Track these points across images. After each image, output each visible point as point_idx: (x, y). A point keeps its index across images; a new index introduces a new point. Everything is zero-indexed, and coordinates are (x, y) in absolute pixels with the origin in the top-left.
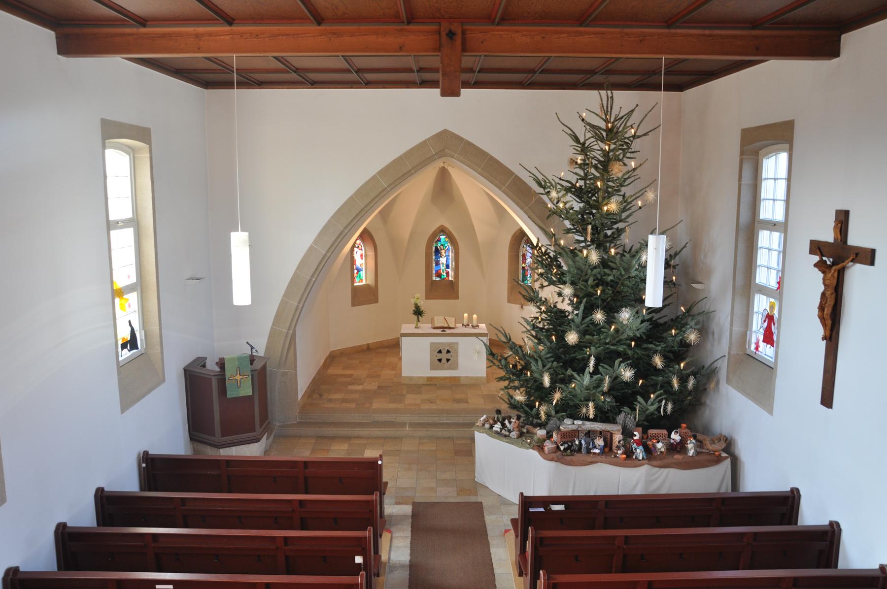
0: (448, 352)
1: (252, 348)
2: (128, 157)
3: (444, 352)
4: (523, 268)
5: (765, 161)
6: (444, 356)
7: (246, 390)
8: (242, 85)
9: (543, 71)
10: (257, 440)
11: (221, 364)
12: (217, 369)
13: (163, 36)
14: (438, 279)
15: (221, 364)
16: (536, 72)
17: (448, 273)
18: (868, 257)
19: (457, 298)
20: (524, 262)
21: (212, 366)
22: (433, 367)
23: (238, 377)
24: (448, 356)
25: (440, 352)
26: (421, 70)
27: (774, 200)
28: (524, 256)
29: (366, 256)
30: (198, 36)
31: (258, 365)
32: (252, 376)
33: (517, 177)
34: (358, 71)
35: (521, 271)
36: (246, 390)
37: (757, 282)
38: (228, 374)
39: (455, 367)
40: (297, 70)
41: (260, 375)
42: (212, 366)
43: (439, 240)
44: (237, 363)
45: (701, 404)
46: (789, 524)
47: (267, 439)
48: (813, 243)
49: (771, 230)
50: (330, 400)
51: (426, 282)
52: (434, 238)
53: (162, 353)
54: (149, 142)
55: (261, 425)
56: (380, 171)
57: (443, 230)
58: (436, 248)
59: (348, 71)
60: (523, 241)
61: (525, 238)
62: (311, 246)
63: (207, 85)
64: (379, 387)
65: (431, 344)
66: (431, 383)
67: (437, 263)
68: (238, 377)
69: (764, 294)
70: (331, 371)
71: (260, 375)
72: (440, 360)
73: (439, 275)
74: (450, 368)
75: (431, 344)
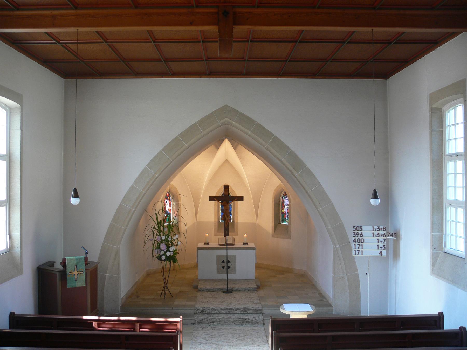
1: (87, 253)
2: (6, 112)
4: (283, 213)
7: (81, 282)
11: (64, 263)
12: (61, 268)
13: (30, 17)
15: (64, 263)
18: (226, 188)
20: (283, 208)
23: (76, 273)
27: (455, 187)
28: (283, 204)
30: (54, 17)
35: (281, 215)
36: (81, 282)
37: (448, 198)
38: (68, 270)
40: (124, 60)
41: (92, 272)
42: (59, 266)
44: (75, 262)
45: (382, 65)
46: (440, 329)
48: (243, 200)
68: (76, 273)
69: (453, 206)
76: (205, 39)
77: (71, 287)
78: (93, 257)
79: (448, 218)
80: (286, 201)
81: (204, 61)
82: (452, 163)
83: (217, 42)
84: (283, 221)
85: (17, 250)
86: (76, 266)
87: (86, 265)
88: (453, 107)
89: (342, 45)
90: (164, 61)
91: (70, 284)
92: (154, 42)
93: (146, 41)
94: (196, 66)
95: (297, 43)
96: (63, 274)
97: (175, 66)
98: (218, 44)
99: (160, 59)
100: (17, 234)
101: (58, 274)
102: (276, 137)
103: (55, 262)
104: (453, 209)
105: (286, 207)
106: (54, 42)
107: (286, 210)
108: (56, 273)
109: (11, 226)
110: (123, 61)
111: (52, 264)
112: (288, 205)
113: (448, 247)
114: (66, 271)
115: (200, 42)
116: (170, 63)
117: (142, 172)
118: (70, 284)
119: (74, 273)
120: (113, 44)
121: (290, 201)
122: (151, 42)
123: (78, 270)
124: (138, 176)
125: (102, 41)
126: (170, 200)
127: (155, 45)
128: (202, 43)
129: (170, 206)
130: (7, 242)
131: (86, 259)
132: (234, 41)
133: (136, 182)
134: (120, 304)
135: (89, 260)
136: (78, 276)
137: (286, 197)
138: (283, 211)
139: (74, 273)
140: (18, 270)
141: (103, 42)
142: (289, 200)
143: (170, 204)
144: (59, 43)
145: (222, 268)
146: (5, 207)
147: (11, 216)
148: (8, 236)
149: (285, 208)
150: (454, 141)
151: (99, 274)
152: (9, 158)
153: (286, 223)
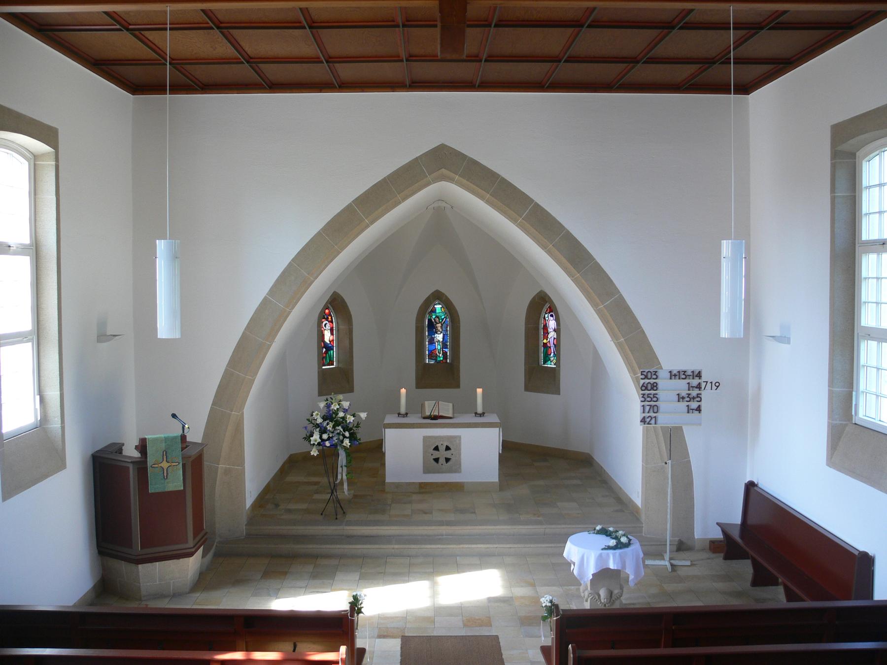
0: (448, 448)
3: (442, 448)
4: (545, 345)
5: (865, 165)
6: (442, 454)
7: (175, 482)
8: (177, 88)
9: (571, 60)
10: (191, 555)
12: (136, 454)
14: (432, 362)
15: (142, 447)
16: (560, 61)
17: (445, 354)
19: (458, 386)
21: (131, 451)
22: (427, 470)
23: (165, 465)
24: (448, 454)
25: (436, 448)
26: (411, 58)
28: (545, 328)
29: (338, 331)
31: (193, 452)
32: (184, 466)
33: (537, 205)
34: (330, 60)
36: (175, 481)
37: (863, 324)
38: (150, 461)
39: (457, 469)
40: (250, 60)
41: (195, 464)
42: (131, 451)
43: (434, 311)
44: (163, 445)
47: (204, 556)
49: (878, 252)
50: (289, 511)
51: (417, 366)
52: (426, 307)
53: (63, 428)
54: (55, 146)
55: (194, 538)
56: (356, 199)
57: (438, 296)
58: (430, 321)
59: (315, 60)
60: (545, 310)
61: (547, 305)
62: (265, 299)
63: (135, 88)
64: (355, 496)
65: (426, 439)
66: (425, 489)
67: (432, 341)
68: (165, 465)
69: (873, 339)
70: (290, 478)
71: (195, 464)
72: (437, 460)
73: (432, 355)
74: (450, 471)
75: (426, 439)
76: (408, 21)
77: (157, 491)
78: (195, 436)
79: (863, 361)
80: (552, 324)
81: (402, 61)
82: (873, 257)
83: (436, 26)
84: (545, 362)
85: (55, 423)
86: (165, 453)
87: (183, 449)
88: (877, 152)
89: (670, 32)
90: (327, 62)
91: (155, 487)
92: (310, 27)
93: (295, 25)
94: (388, 70)
95: (584, 29)
96: (142, 466)
97: (346, 71)
98: (437, 32)
99: (319, 58)
100: (53, 394)
101: (131, 466)
102: (538, 205)
103: (123, 444)
104: (873, 344)
105: (552, 335)
106: (118, 27)
107: (552, 341)
108: (127, 465)
109: (42, 379)
110: (248, 62)
111: (118, 448)
112: (555, 330)
113: (861, 414)
114: (146, 462)
115: (398, 26)
116: (337, 65)
117: (284, 273)
118: (155, 487)
119: (162, 465)
120: (231, 31)
121: (558, 323)
122: (304, 28)
123: (169, 460)
124: (277, 280)
125: (211, 24)
126: (332, 322)
127: (312, 33)
128: (401, 29)
129: (332, 334)
130: (35, 409)
131: (183, 437)
132: (469, 26)
133: (272, 292)
134: (244, 520)
135: (188, 439)
136: (170, 470)
137: (552, 316)
138: (545, 341)
139: (162, 465)
140: (55, 461)
141: (211, 28)
142: (557, 320)
143: (332, 330)
144: (128, 30)
145: (449, 463)
146: (30, 344)
147: (42, 360)
148: (38, 397)
149: (550, 336)
150: (877, 215)
151: (206, 464)
152: (35, 250)
153: (551, 365)
